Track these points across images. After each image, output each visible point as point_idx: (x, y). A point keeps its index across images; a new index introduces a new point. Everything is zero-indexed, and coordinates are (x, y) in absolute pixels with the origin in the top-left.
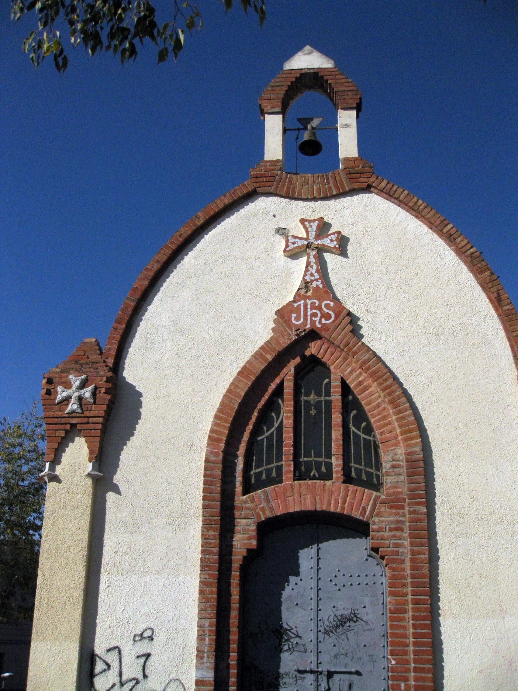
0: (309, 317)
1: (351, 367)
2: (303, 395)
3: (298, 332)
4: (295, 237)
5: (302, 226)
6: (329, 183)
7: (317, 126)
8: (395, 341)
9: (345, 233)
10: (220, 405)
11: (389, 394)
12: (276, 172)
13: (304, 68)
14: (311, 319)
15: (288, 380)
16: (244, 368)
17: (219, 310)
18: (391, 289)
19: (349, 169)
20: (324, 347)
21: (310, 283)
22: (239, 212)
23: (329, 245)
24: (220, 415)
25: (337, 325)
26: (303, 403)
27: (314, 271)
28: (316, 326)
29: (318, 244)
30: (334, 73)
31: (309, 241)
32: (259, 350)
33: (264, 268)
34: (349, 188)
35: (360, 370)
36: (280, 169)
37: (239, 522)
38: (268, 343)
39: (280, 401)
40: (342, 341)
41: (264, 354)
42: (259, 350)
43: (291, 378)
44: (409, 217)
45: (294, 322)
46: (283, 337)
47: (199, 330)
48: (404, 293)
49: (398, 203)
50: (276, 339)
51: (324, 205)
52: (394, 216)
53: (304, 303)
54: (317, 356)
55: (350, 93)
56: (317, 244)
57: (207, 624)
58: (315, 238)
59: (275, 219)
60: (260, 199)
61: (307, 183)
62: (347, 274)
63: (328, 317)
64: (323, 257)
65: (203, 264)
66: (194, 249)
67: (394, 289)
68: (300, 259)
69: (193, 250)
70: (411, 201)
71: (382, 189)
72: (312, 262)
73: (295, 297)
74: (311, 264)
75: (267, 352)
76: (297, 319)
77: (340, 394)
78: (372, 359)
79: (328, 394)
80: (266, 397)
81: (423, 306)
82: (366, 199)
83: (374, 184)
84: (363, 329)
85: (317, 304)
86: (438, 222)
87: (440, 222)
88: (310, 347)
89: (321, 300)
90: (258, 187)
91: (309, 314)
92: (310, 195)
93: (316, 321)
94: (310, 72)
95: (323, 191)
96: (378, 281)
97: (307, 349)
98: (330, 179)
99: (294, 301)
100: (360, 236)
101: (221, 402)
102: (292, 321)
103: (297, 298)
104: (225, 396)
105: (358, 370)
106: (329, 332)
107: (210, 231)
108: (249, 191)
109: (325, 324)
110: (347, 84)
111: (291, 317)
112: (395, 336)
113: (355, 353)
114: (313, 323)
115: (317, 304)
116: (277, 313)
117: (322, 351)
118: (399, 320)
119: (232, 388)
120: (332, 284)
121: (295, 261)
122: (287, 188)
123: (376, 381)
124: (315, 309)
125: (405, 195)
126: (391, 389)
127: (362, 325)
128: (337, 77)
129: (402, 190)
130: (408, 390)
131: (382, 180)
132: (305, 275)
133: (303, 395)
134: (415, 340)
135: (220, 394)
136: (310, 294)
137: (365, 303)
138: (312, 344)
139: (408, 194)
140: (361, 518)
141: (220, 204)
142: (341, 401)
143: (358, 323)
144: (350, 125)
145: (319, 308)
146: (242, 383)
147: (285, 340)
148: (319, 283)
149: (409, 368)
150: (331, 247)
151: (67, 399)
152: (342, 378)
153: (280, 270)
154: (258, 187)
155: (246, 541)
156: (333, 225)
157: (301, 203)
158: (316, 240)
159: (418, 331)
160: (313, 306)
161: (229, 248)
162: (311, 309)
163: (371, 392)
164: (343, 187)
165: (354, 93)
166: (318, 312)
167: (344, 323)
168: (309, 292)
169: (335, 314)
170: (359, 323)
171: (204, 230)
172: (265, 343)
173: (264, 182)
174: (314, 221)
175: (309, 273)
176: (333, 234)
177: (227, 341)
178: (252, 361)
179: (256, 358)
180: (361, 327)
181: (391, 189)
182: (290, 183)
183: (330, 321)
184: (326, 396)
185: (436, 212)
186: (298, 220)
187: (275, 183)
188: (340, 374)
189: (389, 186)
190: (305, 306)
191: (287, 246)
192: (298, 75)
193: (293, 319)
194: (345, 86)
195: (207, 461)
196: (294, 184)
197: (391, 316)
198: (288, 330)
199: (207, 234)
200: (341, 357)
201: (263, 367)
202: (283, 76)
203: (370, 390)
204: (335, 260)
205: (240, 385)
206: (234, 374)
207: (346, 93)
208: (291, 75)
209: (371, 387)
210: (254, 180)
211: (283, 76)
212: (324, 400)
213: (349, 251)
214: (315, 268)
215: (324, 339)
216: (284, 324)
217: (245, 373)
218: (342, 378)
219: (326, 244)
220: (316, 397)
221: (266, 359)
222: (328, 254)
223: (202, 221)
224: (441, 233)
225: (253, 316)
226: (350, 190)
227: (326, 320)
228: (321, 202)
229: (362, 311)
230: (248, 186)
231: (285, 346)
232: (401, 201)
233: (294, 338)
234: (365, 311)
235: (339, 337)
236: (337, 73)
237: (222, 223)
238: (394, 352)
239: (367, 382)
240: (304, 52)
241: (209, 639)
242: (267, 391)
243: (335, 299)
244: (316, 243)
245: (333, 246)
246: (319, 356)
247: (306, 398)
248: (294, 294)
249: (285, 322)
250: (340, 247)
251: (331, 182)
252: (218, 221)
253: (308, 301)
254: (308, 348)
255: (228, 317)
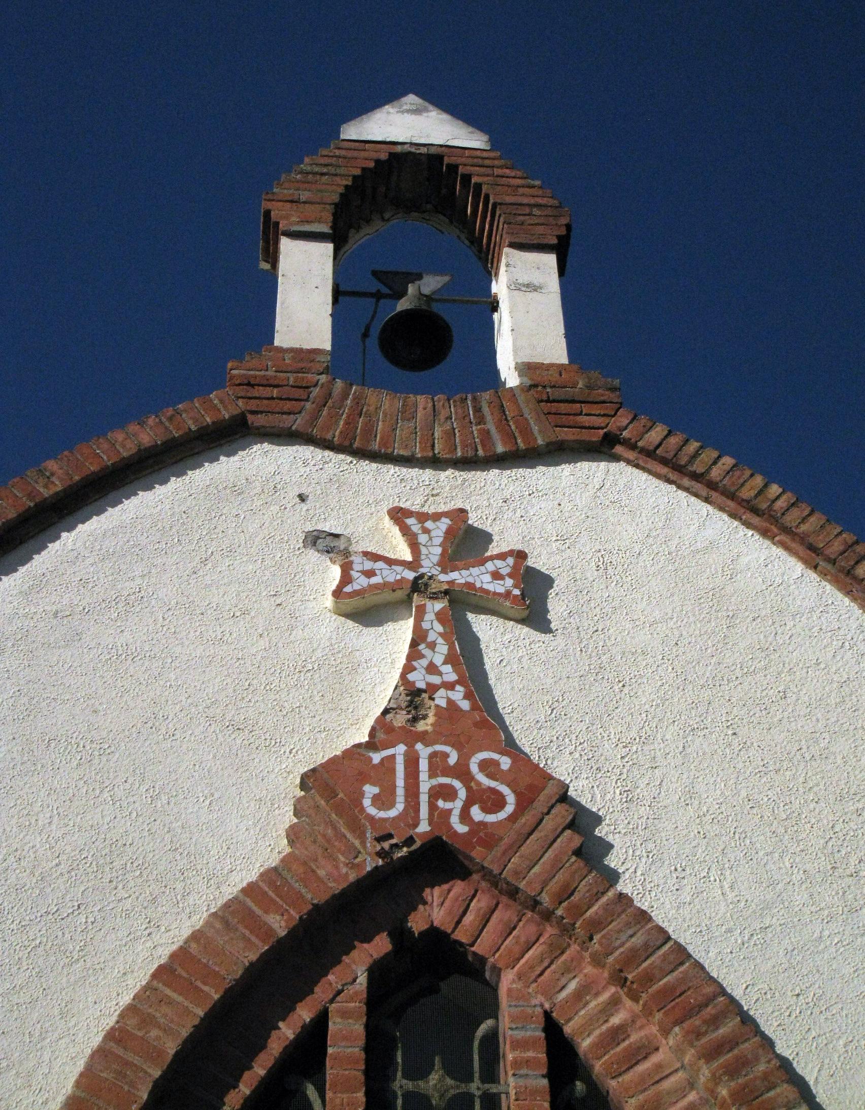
0: (424, 799)
1: (581, 976)
2: (399, 1074)
3: (386, 845)
4: (375, 557)
5: (396, 530)
6: (481, 420)
7: (434, 293)
8: (731, 896)
9: (538, 561)
10: (78, 1084)
11: (732, 1071)
12: (311, 377)
13: (401, 140)
14: (432, 807)
15: (345, 1014)
16: (181, 956)
17: (96, 761)
18: (701, 733)
19: (544, 387)
20: (480, 904)
21: (425, 696)
22: (186, 479)
23: (490, 587)
25: (527, 829)
26: (399, 1102)
27: (438, 660)
28: (449, 827)
29: (452, 583)
30: (487, 162)
31: (422, 570)
32: (241, 897)
33: (263, 644)
34: (548, 440)
35: (613, 989)
36: (326, 371)
38: (271, 876)
39: (311, 1091)
40: (545, 884)
41: (258, 911)
42: (241, 897)
43: (358, 1006)
44: (742, 533)
45: (372, 811)
46: (332, 858)
47: (14, 821)
48: (745, 746)
49: (704, 491)
50: (305, 863)
51: (465, 480)
52: (692, 527)
53: (406, 755)
54: (455, 936)
55: (536, 211)
56: (448, 582)
58: (439, 564)
59: (304, 507)
60: (256, 447)
61: (414, 417)
62: (549, 681)
63: (494, 802)
64: (468, 625)
65: (51, 615)
66: (22, 570)
67: (711, 733)
68: (390, 627)
69: (16, 570)
70: (748, 485)
71: (651, 448)
72: (431, 632)
73: (372, 733)
74: (430, 639)
75: (268, 905)
76: (384, 800)
77: (545, 1071)
78: (659, 948)
79: (490, 1073)
80: (260, 1069)
81: (815, 789)
82: (600, 475)
83: (625, 434)
84: (614, 851)
85: (453, 759)
86: (837, 546)
87: (842, 548)
88: (425, 903)
89: (465, 749)
90: (254, 413)
92: (422, 450)
93: (450, 811)
94: (418, 152)
95: (462, 441)
96: (658, 705)
97: (415, 909)
98: (486, 410)
99: (372, 745)
100: (589, 575)
101: (82, 1075)
102: (363, 809)
103: (381, 735)
104: (100, 1053)
105: (605, 988)
106: (498, 850)
107: (83, 522)
108: (224, 420)
109: (482, 824)
110: (527, 190)
111: (362, 794)
112: (729, 878)
113: (596, 925)
114: (440, 818)
115: (453, 759)
116: (308, 780)
117: (469, 918)
118: (739, 830)
119: (132, 1022)
120: (500, 706)
121: (372, 630)
122: (347, 423)
123: (678, 1022)
124: (445, 774)
125: (727, 468)
126: (736, 1051)
127: (610, 838)
128: (497, 171)
129: (715, 454)
130: (795, 1065)
131: (649, 424)
132: (408, 668)
133: (399, 1074)
134: (801, 897)
135: (77, 1049)
136: (429, 728)
137: (618, 771)
138: (434, 894)
139: (734, 466)
141: (124, 446)
142: (548, 1098)
143: (597, 832)
144: (541, 288)
145: (463, 772)
146: (165, 1009)
147: (337, 867)
148: (458, 694)
149: (790, 987)
150: (495, 593)
152: (547, 1015)
153: (319, 654)
154: (254, 413)
156: (496, 538)
157: (391, 471)
158: (444, 571)
159: (808, 867)
160: (438, 765)
161: (143, 576)
162: (432, 774)
163: (659, 1067)
164: (526, 431)
165: (549, 212)
166: (457, 784)
167: (549, 823)
168: (422, 722)
169: (519, 795)
170: (601, 831)
171: (62, 517)
172: (262, 875)
173: (273, 398)
174: (437, 517)
175: (424, 662)
176: (502, 556)
177: (117, 864)
178: (210, 933)
179: (226, 924)
180: (611, 846)
181: (680, 450)
182: (358, 410)
183: (502, 815)
184: (484, 1080)
185: (828, 520)
186: (385, 510)
187: (308, 405)
188: (539, 1001)
189: (674, 441)
190: (412, 762)
191: (346, 579)
192: (384, 156)
193: (367, 802)
194: (523, 195)
196: (368, 415)
197: (708, 818)
198: (349, 835)
199: (70, 529)
200: (542, 940)
201: (253, 956)
202: (337, 152)
203: (655, 1059)
204: (508, 636)
205: (161, 1014)
206: (140, 978)
207: (527, 211)
208: (363, 154)
209: (657, 1049)
210: (241, 391)
211: (337, 152)
212: (478, 1093)
213: (552, 613)
214: (443, 649)
215: (475, 877)
216: (334, 815)
217: (184, 974)
218: (547, 1015)
219: (478, 585)
220: (449, 1081)
221: (266, 932)
222: (483, 617)
223: (58, 486)
224: (848, 580)
225: (217, 789)
226: (548, 445)
227: (486, 810)
228: (457, 473)
229: (608, 796)
230: (220, 406)
231: (336, 887)
232: (712, 486)
233: (370, 863)
234: (618, 797)
235: (536, 869)
236: (496, 162)
237: (126, 502)
238: (729, 931)
239: (642, 1033)
240: (401, 106)
242: (262, 1046)
243: (511, 747)
244: (443, 577)
245: (501, 590)
246: (460, 935)
247: (409, 1085)
248: (370, 722)
249: (339, 809)
250: (523, 595)
251: (489, 418)
252: (111, 496)
253: (419, 746)
254: (421, 907)
255: (128, 786)
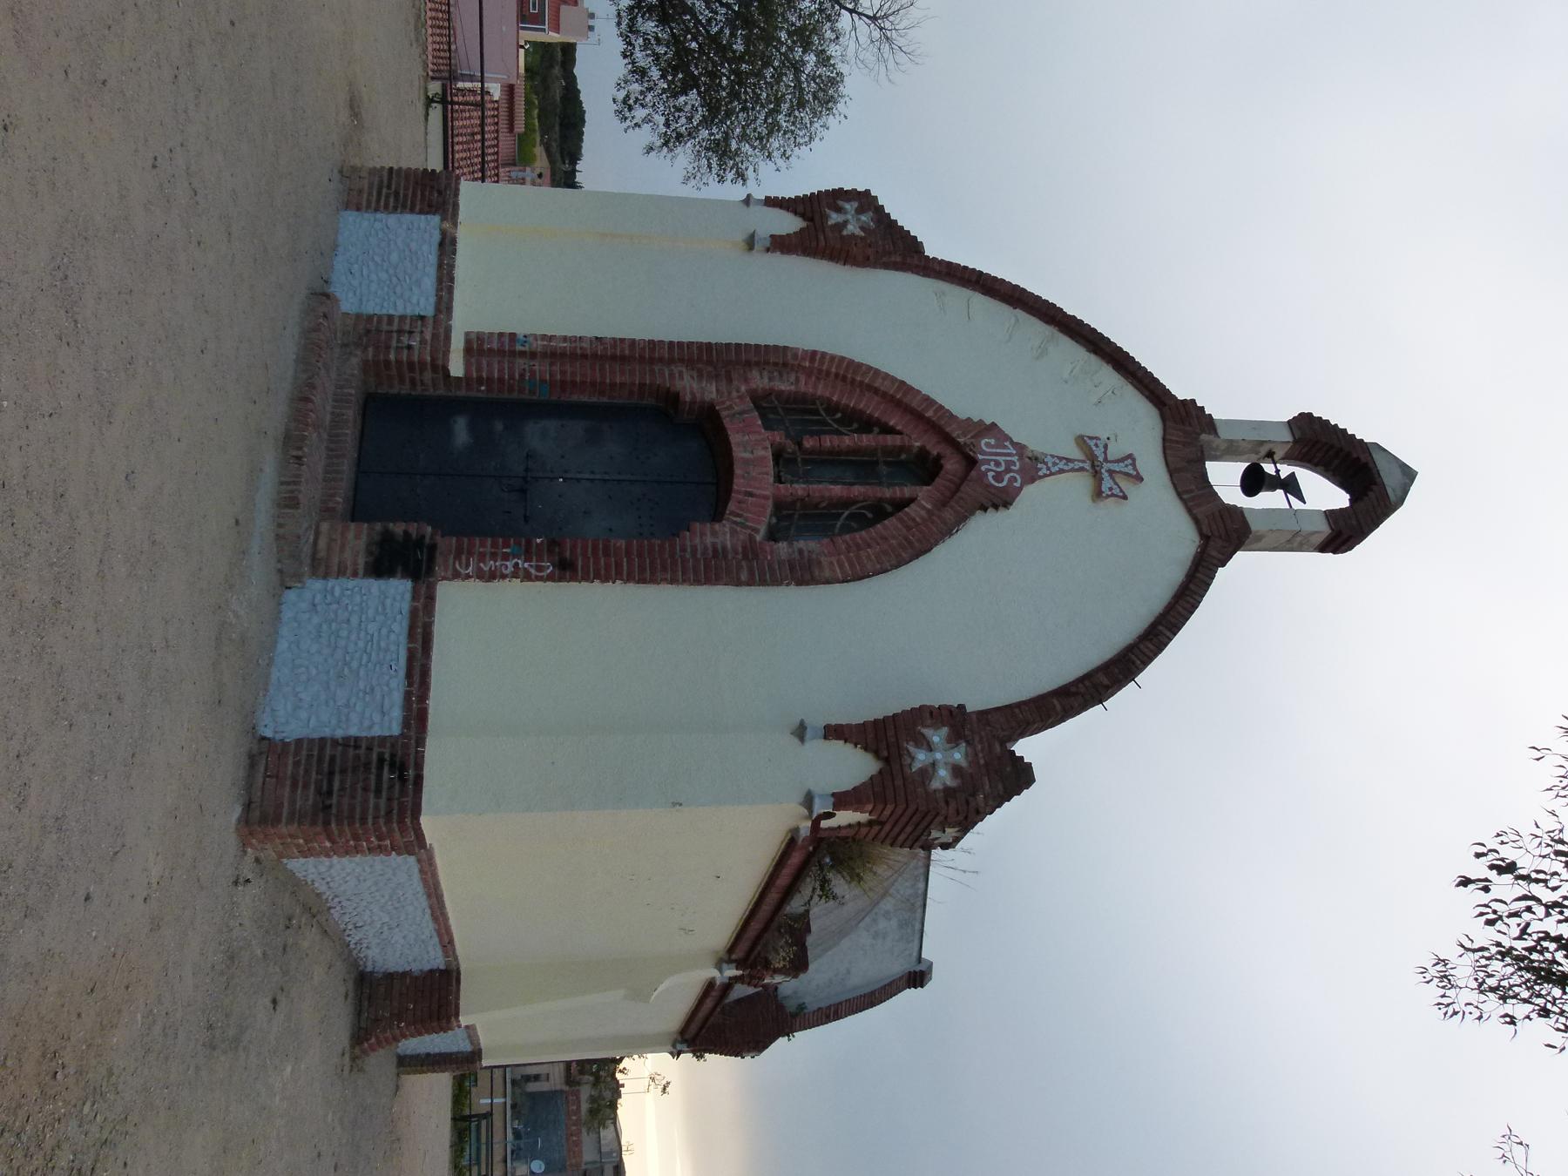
14: (992, 460)
15: (902, 439)
24: (845, 363)
29: (1101, 473)
37: (711, 384)
57: (584, 345)
63: (998, 477)
75: (936, 411)
76: (988, 445)
91: (998, 458)
114: (988, 462)
115: (1013, 467)
132: (1053, 456)
140: (728, 512)
145: (1008, 470)
151: (930, 748)
155: (688, 391)
162: (1006, 461)
175: (1058, 461)
183: (993, 482)
195: (786, 348)
241: (565, 347)
244: (1103, 471)
